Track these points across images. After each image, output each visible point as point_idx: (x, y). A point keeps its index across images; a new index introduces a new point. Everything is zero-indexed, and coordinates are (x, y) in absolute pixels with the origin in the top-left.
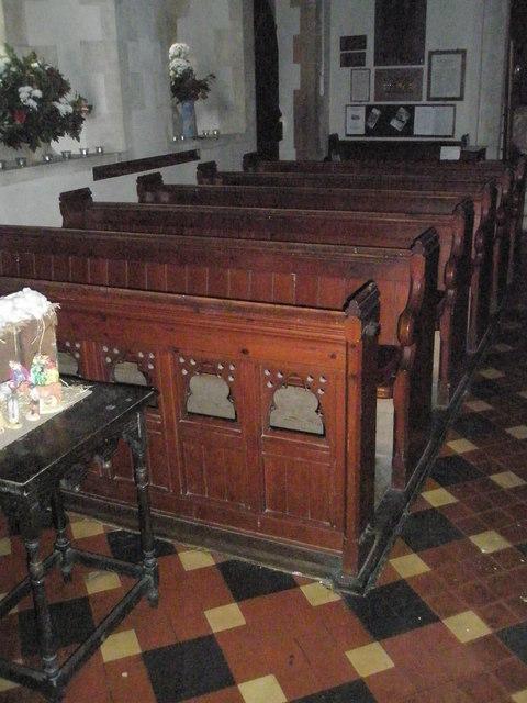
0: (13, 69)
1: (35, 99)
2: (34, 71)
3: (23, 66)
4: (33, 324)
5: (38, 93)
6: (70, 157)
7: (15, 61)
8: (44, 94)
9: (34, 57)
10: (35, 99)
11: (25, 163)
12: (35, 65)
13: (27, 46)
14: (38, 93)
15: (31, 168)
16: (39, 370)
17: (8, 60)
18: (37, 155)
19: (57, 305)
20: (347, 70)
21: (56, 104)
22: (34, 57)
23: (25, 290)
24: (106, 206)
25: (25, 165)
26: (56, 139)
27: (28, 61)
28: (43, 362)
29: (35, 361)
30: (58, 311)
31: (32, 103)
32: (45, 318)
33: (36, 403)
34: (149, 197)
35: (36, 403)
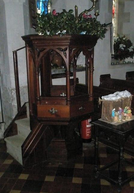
0: (119, 40)
1: (123, 47)
2: (124, 40)
3: (121, 39)
4: (127, 98)
5: (124, 46)
6: (130, 63)
7: (120, 38)
8: (126, 47)
9: (124, 36)
10: (123, 47)
11: (113, 64)
12: (124, 39)
13: (122, 34)
14: (124, 46)
15: (120, 65)
16: (126, 110)
17: (118, 38)
18: (121, 62)
19: (133, 95)
20: (23, 43)
21: (128, 49)
22: (124, 36)
23: (126, 91)
24: (115, 80)
25: (119, 64)
26: (127, 58)
27: (123, 38)
28: (127, 108)
29: (126, 108)
30: (132, 96)
31: (123, 48)
32: (130, 98)
33: (126, 117)
34: (129, 78)
35: (126, 117)
